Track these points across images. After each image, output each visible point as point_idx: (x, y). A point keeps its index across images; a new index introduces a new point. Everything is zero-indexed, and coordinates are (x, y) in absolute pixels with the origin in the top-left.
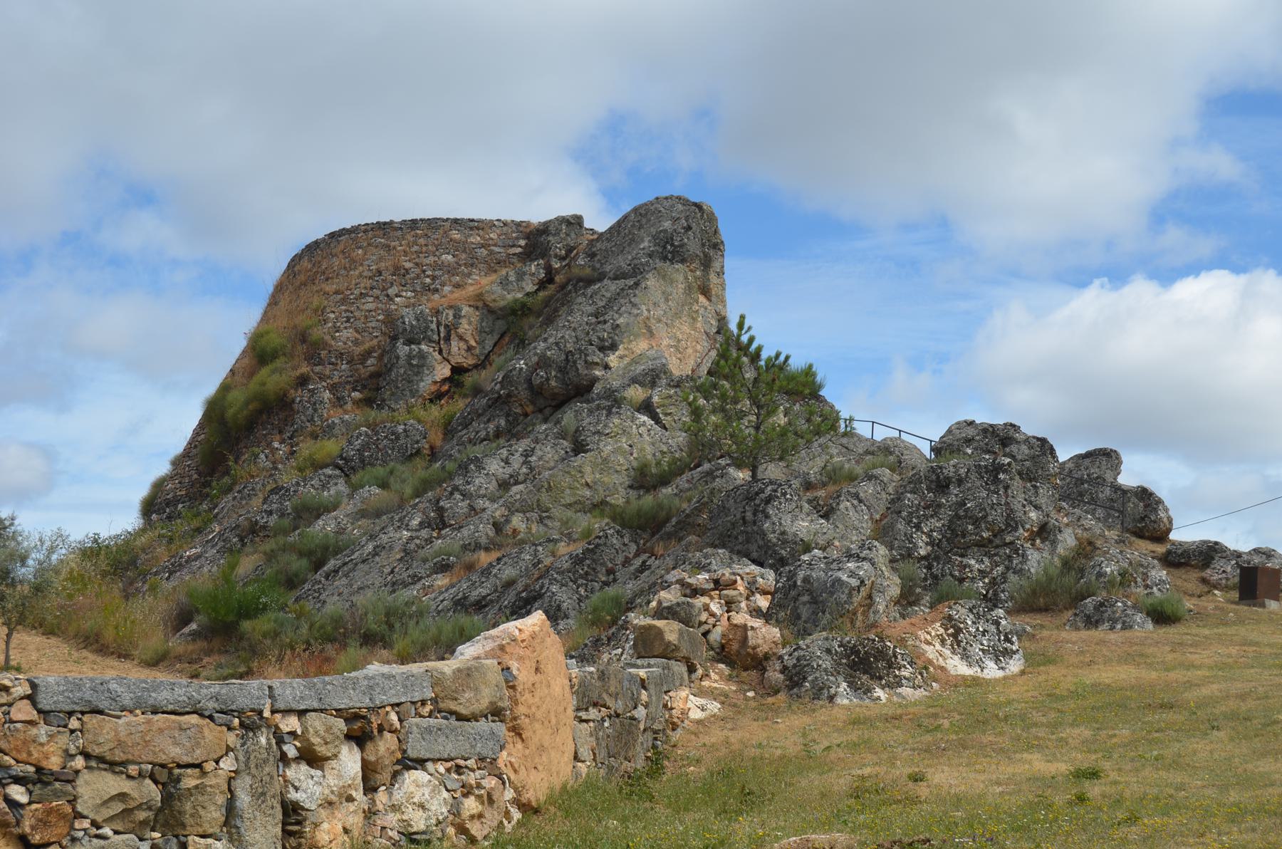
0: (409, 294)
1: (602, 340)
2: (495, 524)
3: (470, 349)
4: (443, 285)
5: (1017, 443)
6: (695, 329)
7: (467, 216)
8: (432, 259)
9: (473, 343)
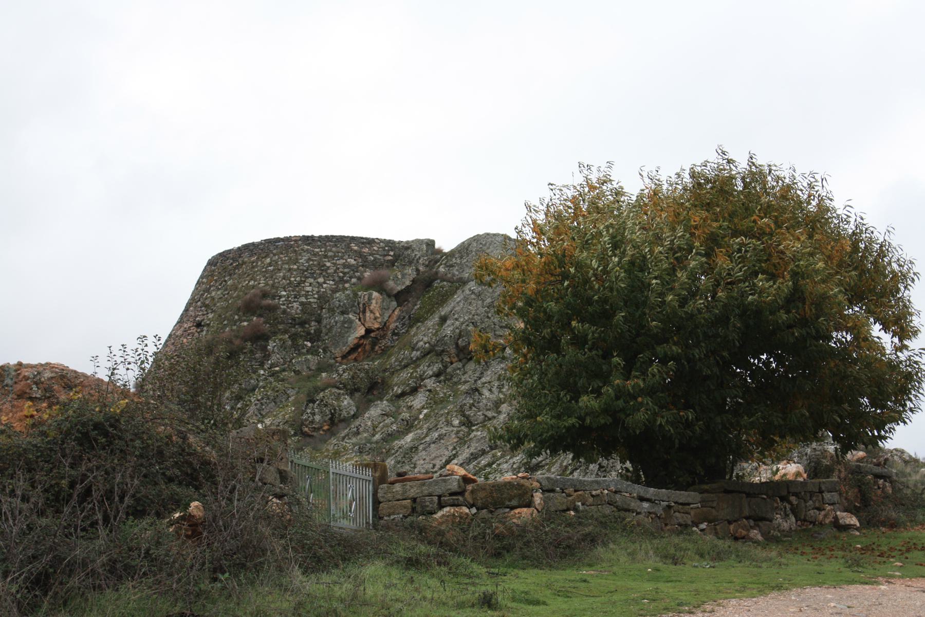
0: (331, 282)
3: (376, 318)
4: (351, 278)
8: (342, 261)
9: (378, 315)
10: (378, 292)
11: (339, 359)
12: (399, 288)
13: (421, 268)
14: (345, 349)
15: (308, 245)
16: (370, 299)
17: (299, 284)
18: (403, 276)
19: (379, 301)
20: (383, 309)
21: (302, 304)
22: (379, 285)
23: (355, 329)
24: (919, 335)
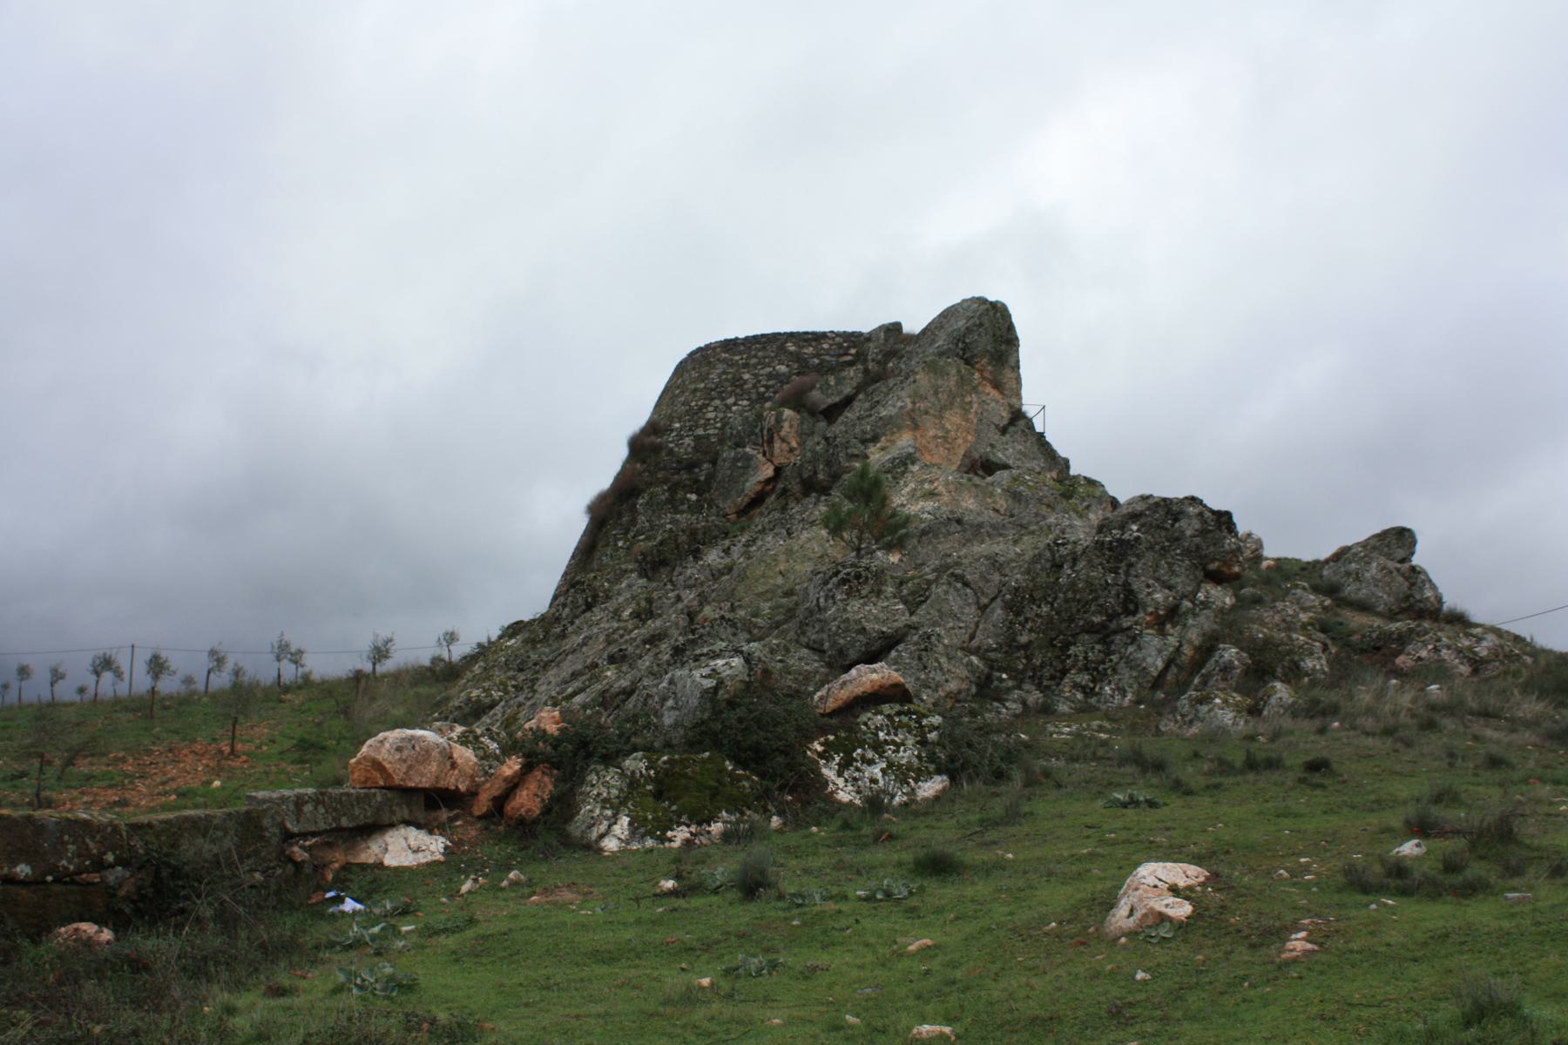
1: (864, 432)
2: (689, 614)
3: (791, 450)
5: (1189, 517)
6: (967, 420)
7: (802, 330)
9: (794, 444)
10: (794, 409)
11: (733, 517)
12: (830, 401)
13: (871, 366)
14: (742, 501)
15: (726, 351)
16: (779, 420)
17: (700, 409)
18: (839, 381)
19: (795, 424)
20: (803, 436)
21: (698, 439)
22: (798, 401)
23: (756, 468)
24: (163, 655)
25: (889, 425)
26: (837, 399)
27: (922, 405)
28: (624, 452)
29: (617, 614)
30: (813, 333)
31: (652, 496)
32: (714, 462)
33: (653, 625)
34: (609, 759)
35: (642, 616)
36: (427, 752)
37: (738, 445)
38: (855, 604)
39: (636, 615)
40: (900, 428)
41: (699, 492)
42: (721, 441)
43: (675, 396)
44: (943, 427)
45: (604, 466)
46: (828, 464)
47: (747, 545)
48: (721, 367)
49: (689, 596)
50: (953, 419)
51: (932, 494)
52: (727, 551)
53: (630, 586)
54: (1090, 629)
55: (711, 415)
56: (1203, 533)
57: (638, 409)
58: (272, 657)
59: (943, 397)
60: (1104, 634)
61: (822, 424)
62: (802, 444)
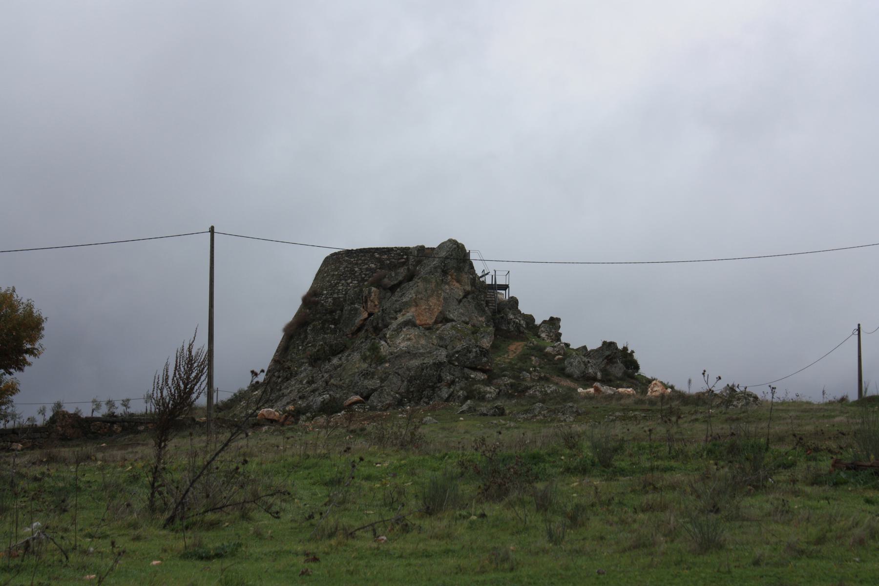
3: (375, 306)
14: (354, 328)
16: (370, 293)
18: (396, 274)
20: (381, 299)
21: (334, 299)
22: (378, 284)
25: (406, 305)
26: (396, 282)
27: (420, 296)
28: (300, 303)
29: (301, 382)
30: (387, 248)
31: (314, 326)
32: (342, 311)
33: (314, 386)
34: (304, 414)
35: (310, 383)
36: (271, 413)
37: (352, 303)
38: (366, 381)
39: (308, 382)
40: (410, 306)
41: (335, 324)
42: (345, 300)
43: (324, 277)
44: (429, 305)
45: (289, 309)
46: (383, 320)
47: (347, 356)
48: (345, 264)
49: (326, 376)
50: (433, 301)
51: (409, 339)
52: (340, 359)
53: (305, 370)
54: (429, 387)
55: (340, 288)
56: (476, 357)
57: (305, 283)
58: (143, 401)
59: (429, 292)
60: (433, 388)
61: (389, 294)
62: (380, 303)
